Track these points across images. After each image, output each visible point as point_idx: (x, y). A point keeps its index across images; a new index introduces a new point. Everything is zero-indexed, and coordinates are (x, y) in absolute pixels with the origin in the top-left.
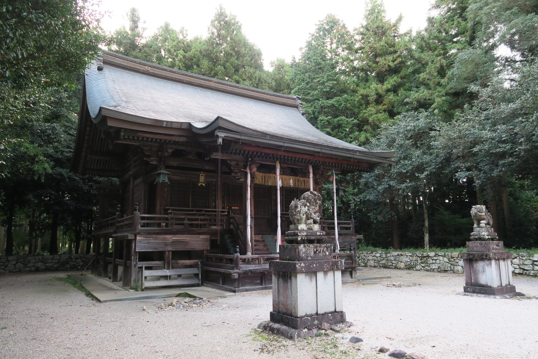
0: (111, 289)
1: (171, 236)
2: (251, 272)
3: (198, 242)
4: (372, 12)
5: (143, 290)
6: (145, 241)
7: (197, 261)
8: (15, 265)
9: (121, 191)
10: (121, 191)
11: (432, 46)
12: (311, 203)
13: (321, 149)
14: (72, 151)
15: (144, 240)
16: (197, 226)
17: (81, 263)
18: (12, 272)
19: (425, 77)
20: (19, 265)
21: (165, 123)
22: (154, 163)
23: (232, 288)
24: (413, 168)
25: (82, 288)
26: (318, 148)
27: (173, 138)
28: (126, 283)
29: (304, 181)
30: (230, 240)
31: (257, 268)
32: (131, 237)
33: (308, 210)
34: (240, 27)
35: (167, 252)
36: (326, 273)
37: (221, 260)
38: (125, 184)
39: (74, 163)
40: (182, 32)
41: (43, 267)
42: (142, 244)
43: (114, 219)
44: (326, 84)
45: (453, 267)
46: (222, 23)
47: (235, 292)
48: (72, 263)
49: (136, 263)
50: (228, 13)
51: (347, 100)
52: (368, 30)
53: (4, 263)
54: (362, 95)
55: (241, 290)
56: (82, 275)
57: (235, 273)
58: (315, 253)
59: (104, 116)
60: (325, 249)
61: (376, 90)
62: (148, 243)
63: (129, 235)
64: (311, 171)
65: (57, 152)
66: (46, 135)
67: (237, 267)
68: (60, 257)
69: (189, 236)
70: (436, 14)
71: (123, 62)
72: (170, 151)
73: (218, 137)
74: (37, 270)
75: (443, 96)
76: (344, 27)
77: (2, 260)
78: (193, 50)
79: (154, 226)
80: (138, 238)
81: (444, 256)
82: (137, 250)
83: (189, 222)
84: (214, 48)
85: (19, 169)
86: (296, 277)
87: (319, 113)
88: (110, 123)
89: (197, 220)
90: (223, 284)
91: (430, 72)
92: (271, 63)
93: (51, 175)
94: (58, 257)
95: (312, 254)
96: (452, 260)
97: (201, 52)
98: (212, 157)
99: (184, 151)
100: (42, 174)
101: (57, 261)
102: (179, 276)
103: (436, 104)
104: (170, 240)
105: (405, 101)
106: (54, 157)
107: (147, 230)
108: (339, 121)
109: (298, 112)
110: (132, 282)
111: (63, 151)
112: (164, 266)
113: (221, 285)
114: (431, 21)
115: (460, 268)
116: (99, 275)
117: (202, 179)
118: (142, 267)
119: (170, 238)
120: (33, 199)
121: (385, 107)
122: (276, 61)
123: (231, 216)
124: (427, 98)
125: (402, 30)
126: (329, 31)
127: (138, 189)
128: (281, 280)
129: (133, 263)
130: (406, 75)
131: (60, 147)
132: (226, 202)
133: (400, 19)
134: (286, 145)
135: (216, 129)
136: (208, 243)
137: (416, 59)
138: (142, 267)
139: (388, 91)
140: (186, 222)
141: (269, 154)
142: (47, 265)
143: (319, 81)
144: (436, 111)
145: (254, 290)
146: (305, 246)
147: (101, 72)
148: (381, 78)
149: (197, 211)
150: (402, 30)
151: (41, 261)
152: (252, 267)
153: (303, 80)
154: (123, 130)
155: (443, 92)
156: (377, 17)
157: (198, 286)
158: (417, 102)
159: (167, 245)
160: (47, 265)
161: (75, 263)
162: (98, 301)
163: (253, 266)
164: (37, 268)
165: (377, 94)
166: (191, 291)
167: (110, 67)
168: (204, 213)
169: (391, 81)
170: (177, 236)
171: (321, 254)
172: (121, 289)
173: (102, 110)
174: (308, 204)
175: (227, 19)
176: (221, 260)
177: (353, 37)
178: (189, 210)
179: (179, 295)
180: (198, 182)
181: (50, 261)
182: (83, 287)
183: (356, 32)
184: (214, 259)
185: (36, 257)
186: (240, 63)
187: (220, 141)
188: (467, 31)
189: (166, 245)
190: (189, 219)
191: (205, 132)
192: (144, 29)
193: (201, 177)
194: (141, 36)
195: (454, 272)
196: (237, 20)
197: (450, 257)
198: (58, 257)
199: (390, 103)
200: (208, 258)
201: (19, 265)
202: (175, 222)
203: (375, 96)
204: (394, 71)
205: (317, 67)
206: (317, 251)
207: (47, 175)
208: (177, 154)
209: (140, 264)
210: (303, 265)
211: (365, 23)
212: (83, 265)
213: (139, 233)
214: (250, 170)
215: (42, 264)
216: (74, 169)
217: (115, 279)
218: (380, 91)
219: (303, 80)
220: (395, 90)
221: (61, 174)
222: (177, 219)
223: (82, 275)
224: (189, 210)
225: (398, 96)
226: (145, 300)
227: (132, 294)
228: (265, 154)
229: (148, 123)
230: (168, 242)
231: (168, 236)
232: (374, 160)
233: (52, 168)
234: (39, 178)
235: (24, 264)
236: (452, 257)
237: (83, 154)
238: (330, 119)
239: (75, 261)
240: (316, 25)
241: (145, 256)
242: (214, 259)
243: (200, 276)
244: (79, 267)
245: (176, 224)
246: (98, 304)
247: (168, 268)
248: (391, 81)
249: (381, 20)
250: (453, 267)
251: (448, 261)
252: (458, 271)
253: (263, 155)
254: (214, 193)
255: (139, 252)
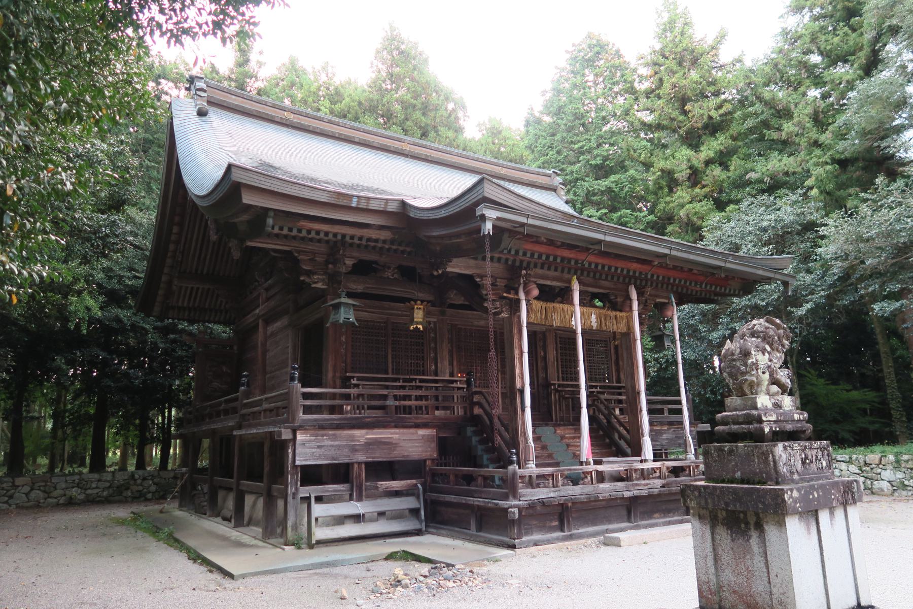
0: (239, 545)
1: (363, 432)
2: (543, 503)
3: (413, 442)
4: (670, 26)
5: (311, 546)
6: (313, 444)
7: (414, 481)
8: (27, 494)
9: (235, 348)
10: (235, 348)
11: (792, 79)
12: (775, 345)
13: (671, 249)
14: (142, 275)
15: (310, 441)
16: (408, 410)
17: (153, 488)
18: (23, 508)
19: (791, 129)
20: (37, 494)
21: (355, 199)
22: (320, 285)
23: (506, 539)
24: (779, 297)
25: (175, 543)
26: (666, 247)
27: (366, 233)
28: (274, 529)
29: (616, 317)
30: (477, 438)
31: (552, 495)
32: (286, 435)
33: (771, 361)
34: (426, 60)
35: (356, 466)
36: (832, 510)
37: (469, 479)
38: (245, 336)
39: (145, 298)
40: (324, 69)
41: (82, 497)
42: (308, 449)
43: (236, 399)
44: (595, 152)
45: (869, 482)
46: (395, 53)
47: (513, 547)
48: (135, 488)
49: (297, 489)
50: (404, 36)
51: (634, 180)
52: (664, 56)
53: (8, 491)
54: (662, 170)
55: (524, 542)
56: (161, 512)
57: (513, 506)
58: (804, 463)
59: (234, 182)
60: (820, 453)
61: (689, 160)
62: (319, 447)
63: (283, 430)
64: (634, 295)
65: (110, 278)
66: (99, 237)
67: (515, 495)
68: (113, 476)
69: (397, 430)
70: (794, 22)
71: (242, 102)
72: (349, 262)
73: (483, 218)
74: (70, 504)
75: (827, 163)
76: (618, 54)
77: (4, 485)
78: (347, 99)
79: (321, 413)
80: (300, 437)
81: (850, 462)
82: (298, 463)
83: (397, 403)
84: (383, 97)
85: (44, 307)
86: (781, 524)
87: (582, 203)
88: (248, 199)
89: (408, 397)
90: (479, 529)
91: (799, 123)
92: (479, 125)
93: (99, 321)
94: (109, 478)
95: (799, 465)
96: (868, 469)
97: (360, 103)
98: (449, 269)
99: (376, 262)
100: (83, 318)
101: (108, 484)
102: (381, 514)
103: (813, 178)
104: (363, 441)
105: (747, 177)
106: (105, 288)
107: (316, 420)
108: (621, 217)
109: (558, 199)
110: (289, 529)
111: (121, 277)
112: (351, 495)
113: (473, 531)
114: (785, 33)
115: (885, 485)
116: (200, 512)
117: (419, 315)
118: (309, 498)
119: (362, 435)
120: (64, 367)
121: (707, 190)
122: (487, 122)
123: (474, 389)
124: (791, 170)
125: (725, 56)
126: (590, 63)
127: (279, 343)
128: (723, 534)
129: (291, 490)
130: (740, 134)
131: (116, 268)
132: (455, 363)
133: (721, 37)
134: (609, 239)
135: (477, 204)
136: (434, 445)
137: (766, 103)
138: (309, 498)
139: (708, 163)
140: (390, 402)
141: (569, 260)
142: (89, 492)
143: (581, 147)
144: (815, 192)
145: (549, 542)
146: (785, 448)
147: (204, 118)
148: (692, 140)
149: (405, 380)
150: (725, 56)
151: (78, 486)
152: (542, 493)
153: (551, 147)
154: (271, 214)
155: (826, 158)
156: (682, 33)
157: (418, 535)
158: (771, 179)
159: (356, 450)
160: (89, 492)
161: (141, 488)
162: (231, 576)
163: (545, 490)
164: (71, 498)
165: (691, 168)
166: (414, 545)
167: (219, 111)
168: (418, 384)
169: (711, 147)
170: (376, 431)
171: (814, 467)
172: (261, 543)
173: (233, 170)
174: (768, 348)
175: (403, 47)
176: (469, 479)
177: (635, 70)
178: (386, 380)
179: (390, 557)
180: (412, 321)
181: (94, 485)
182: (177, 540)
183: (642, 61)
184: (452, 478)
185: (68, 478)
186: (429, 122)
187: (488, 227)
188: (861, 49)
189: (354, 449)
190: (396, 398)
191: (443, 213)
192: (260, 64)
193: (416, 311)
194: (256, 77)
195: (873, 493)
196: (420, 49)
197: (862, 464)
198: (109, 477)
199: (715, 182)
200: (434, 474)
201: (37, 494)
202: (366, 403)
203: (689, 171)
204: (713, 128)
205: (577, 122)
206: (806, 458)
207: (92, 321)
208: (363, 269)
209: (304, 491)
210: (796, 494)
211: (658, 46)
212: (156, 491)
213: (301, 427)
214: (527, 293)
215: (79, 491)
216: (145, 305)
217: (238, 518)
218: (695, 162)
219: (551, 147)
220: (722, 159)
221: (118, 320)
222: (372, 397)
223: (161, 512)
224: (386, 380)
225: (728, 170)
226: (326, 570)
227: (289, 556)
228: (563, 259)
229: (324, 198)
230: (356, 443)
231: (357, 433)
232: (760, 272)
233: (101, 308)
234: (78, 326)
235: (45, 492)
236: (866, 464)
237: (164, 278)
238: (605, 214)
239: (141, 484)
240: (567, 52)
241: (312, 475)
242: (452, 478)
243: (422, 513)
244: (149, 496)
245: (370, 408)
246: (227, 582)
247: (360, 499)
248: (711, 147)
249: (690, 37)
250: (869, 482)
251: (858, 471)
252: (882, 490)
253: (559, 260)
254: (433, 345)
255: (303, 467)
